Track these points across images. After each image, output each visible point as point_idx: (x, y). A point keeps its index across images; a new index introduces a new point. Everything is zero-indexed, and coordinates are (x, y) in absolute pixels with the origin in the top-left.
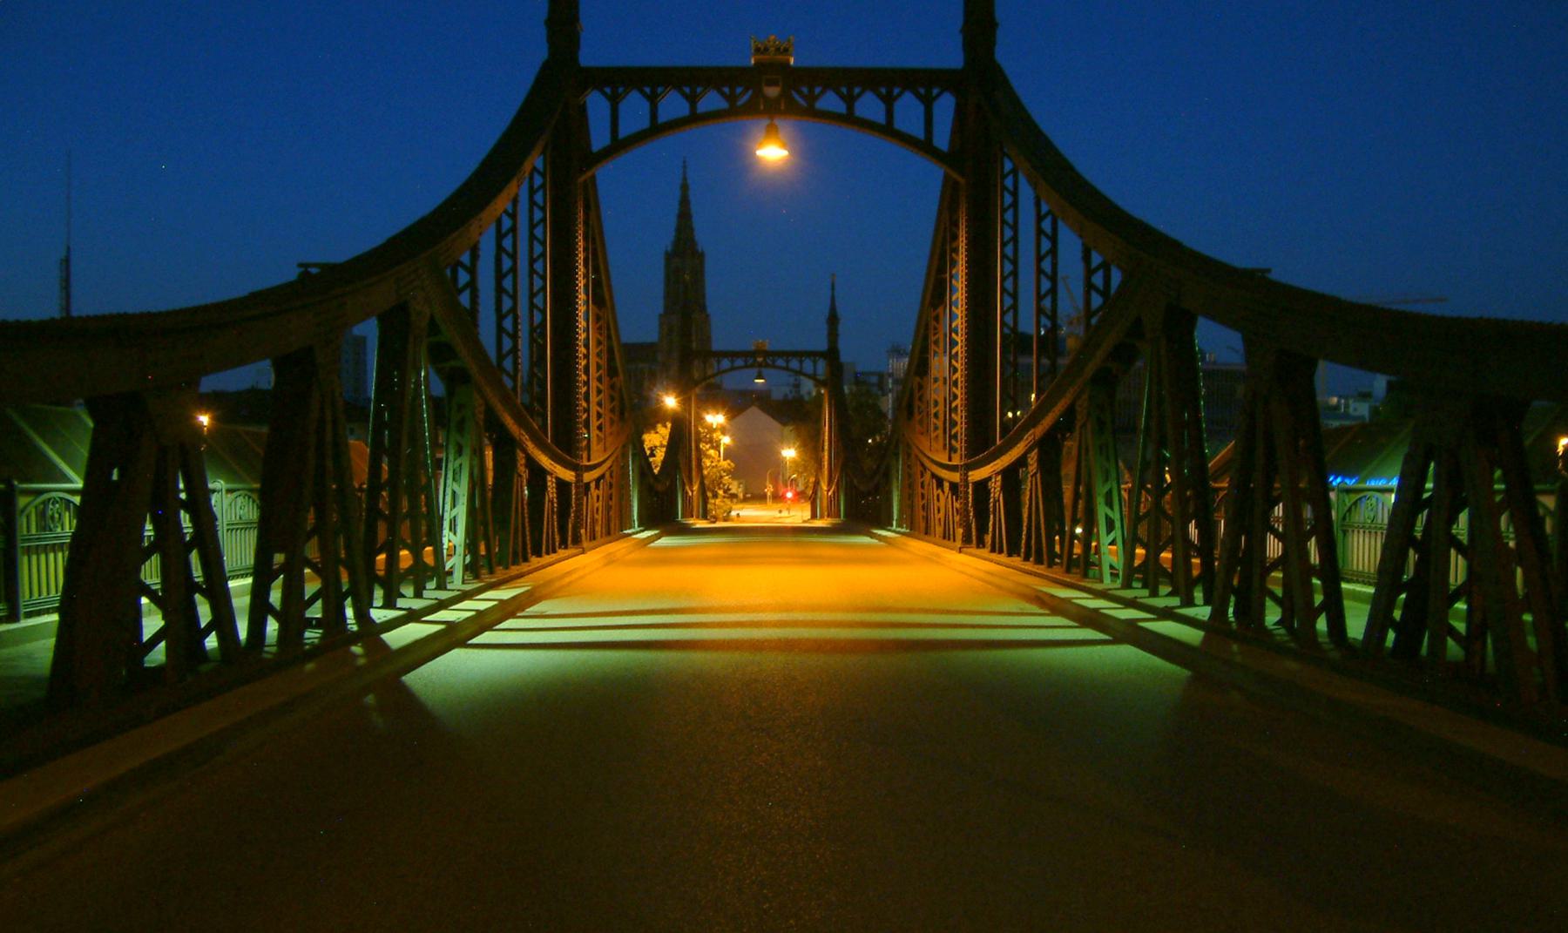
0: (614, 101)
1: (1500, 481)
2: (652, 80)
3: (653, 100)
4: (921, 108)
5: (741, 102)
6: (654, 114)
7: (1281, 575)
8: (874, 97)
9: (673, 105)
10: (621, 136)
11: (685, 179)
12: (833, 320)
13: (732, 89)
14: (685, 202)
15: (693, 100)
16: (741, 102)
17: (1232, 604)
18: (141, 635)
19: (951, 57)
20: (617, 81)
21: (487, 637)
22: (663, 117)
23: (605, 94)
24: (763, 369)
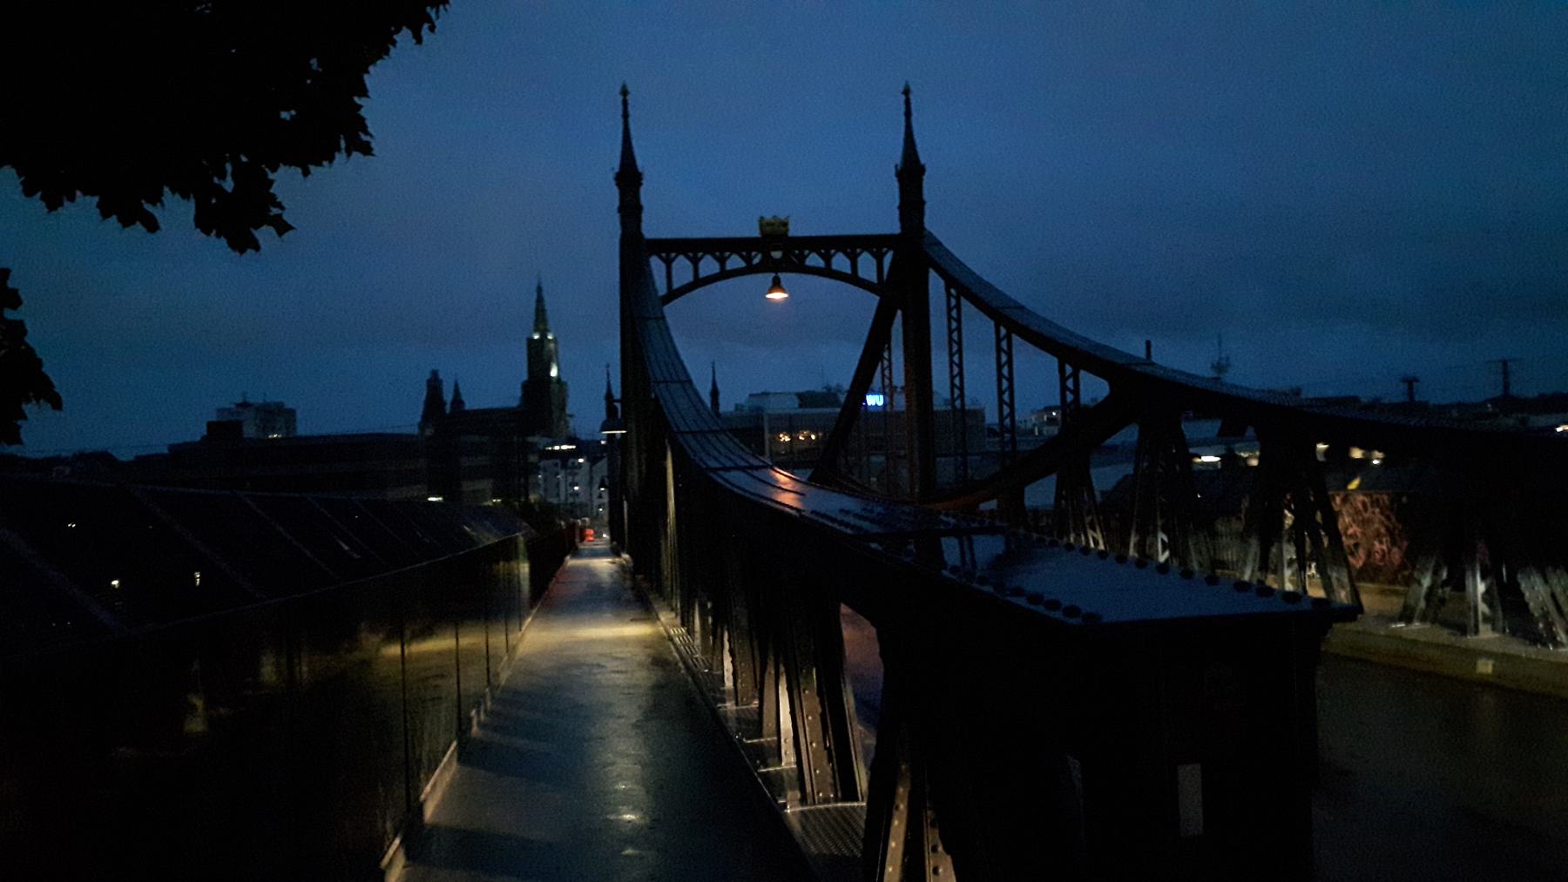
0: (668, 263)
2: (693, 248)
3: (695, 262)
5: (756, 261)
7: (1246, 577)
9: (709, 266)
12: (911, 174)
13: (722, 253)
14: (540, 300)
15: (722, 261)
16: (756, 261)
17: (571, 447)
19: (892, 226)
20: (670, 248)
22: (703, 274)
23: (661, 258)
24: (782, 276)
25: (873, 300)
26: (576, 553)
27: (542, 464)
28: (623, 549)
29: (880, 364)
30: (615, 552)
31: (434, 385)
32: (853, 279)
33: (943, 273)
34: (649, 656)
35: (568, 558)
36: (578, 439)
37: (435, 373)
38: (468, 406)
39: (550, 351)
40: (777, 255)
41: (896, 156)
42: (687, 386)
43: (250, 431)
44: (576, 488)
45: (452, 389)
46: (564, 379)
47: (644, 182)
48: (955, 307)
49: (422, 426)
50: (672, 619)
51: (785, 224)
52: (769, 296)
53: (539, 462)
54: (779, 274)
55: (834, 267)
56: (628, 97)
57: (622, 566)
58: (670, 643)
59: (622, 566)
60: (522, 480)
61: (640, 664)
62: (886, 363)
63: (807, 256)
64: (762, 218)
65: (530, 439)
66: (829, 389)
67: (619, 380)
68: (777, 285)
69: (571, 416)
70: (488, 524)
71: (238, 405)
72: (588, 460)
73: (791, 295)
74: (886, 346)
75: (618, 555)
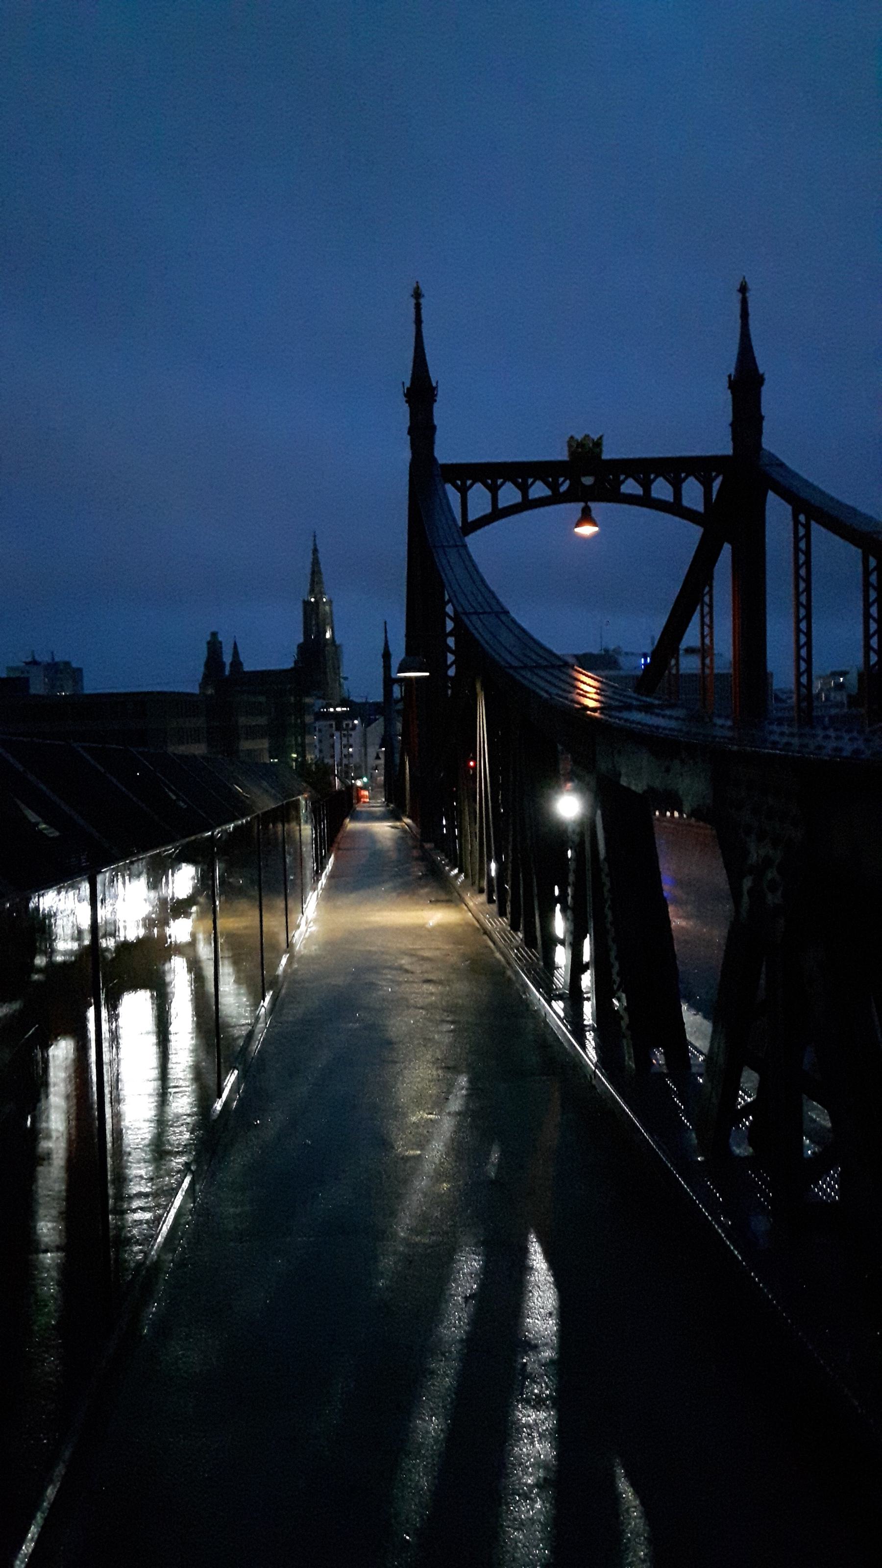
0: (463, 491)
1: (806, 1139)
3: (494, 490)
4: (488, 494)
5: (563, 488)
6: (525, 494)
8: (512, 486)
10: (500, 506)
11: (315, 545)
14: (316, 563)
15: (524, 489)
16: (563, 488)
18: (456, 667)
21: (551, 671)
24: (592, 505)
25: (696, 532)
26: (356, 817)
27: (317, 724)
28: (404, 813)
29: (699, 607)
30: (394, 815)
31: (214, 647)
32: (676, 508)
33: (787, 494)
34: (463, 955)
35: (348, 820)
36: (352, 701)
37: (214, 635)
38: (247, 667)
39: (325, 614)
40: (588, 481)
41: (729, 364)
42: (503, 618)
43: (38, 687)
44: (351, 750)
45: (231, 651)
46: (338, 642)
47: (438, 398)
48: (804, 536)
49: (203, 685)
50: (482, 904)
51: (598, 444)
52: (577, 530)
53: (315, 722)
54: (590, 504)
55: (654, 494)
56: (422, 301)
57: (404, 831)
58: (485, 937)
59: (404, 831)
60: (299, 739)
61: (455, 969)
62: (706, 609)
63: (623, 482)
64: (572, 437)
65: (307, 700)
66: (606, 651)
67: (403, 631)
68: (586, 517)
69: (346, 679)
70: (265, 784)
71: (27, 663)
72: (362, 722)
73: (601, 529)
74: (707, 589)
75: (399, 819)
